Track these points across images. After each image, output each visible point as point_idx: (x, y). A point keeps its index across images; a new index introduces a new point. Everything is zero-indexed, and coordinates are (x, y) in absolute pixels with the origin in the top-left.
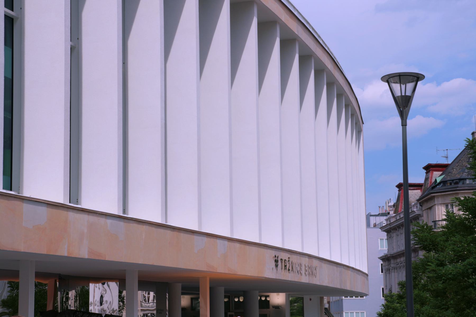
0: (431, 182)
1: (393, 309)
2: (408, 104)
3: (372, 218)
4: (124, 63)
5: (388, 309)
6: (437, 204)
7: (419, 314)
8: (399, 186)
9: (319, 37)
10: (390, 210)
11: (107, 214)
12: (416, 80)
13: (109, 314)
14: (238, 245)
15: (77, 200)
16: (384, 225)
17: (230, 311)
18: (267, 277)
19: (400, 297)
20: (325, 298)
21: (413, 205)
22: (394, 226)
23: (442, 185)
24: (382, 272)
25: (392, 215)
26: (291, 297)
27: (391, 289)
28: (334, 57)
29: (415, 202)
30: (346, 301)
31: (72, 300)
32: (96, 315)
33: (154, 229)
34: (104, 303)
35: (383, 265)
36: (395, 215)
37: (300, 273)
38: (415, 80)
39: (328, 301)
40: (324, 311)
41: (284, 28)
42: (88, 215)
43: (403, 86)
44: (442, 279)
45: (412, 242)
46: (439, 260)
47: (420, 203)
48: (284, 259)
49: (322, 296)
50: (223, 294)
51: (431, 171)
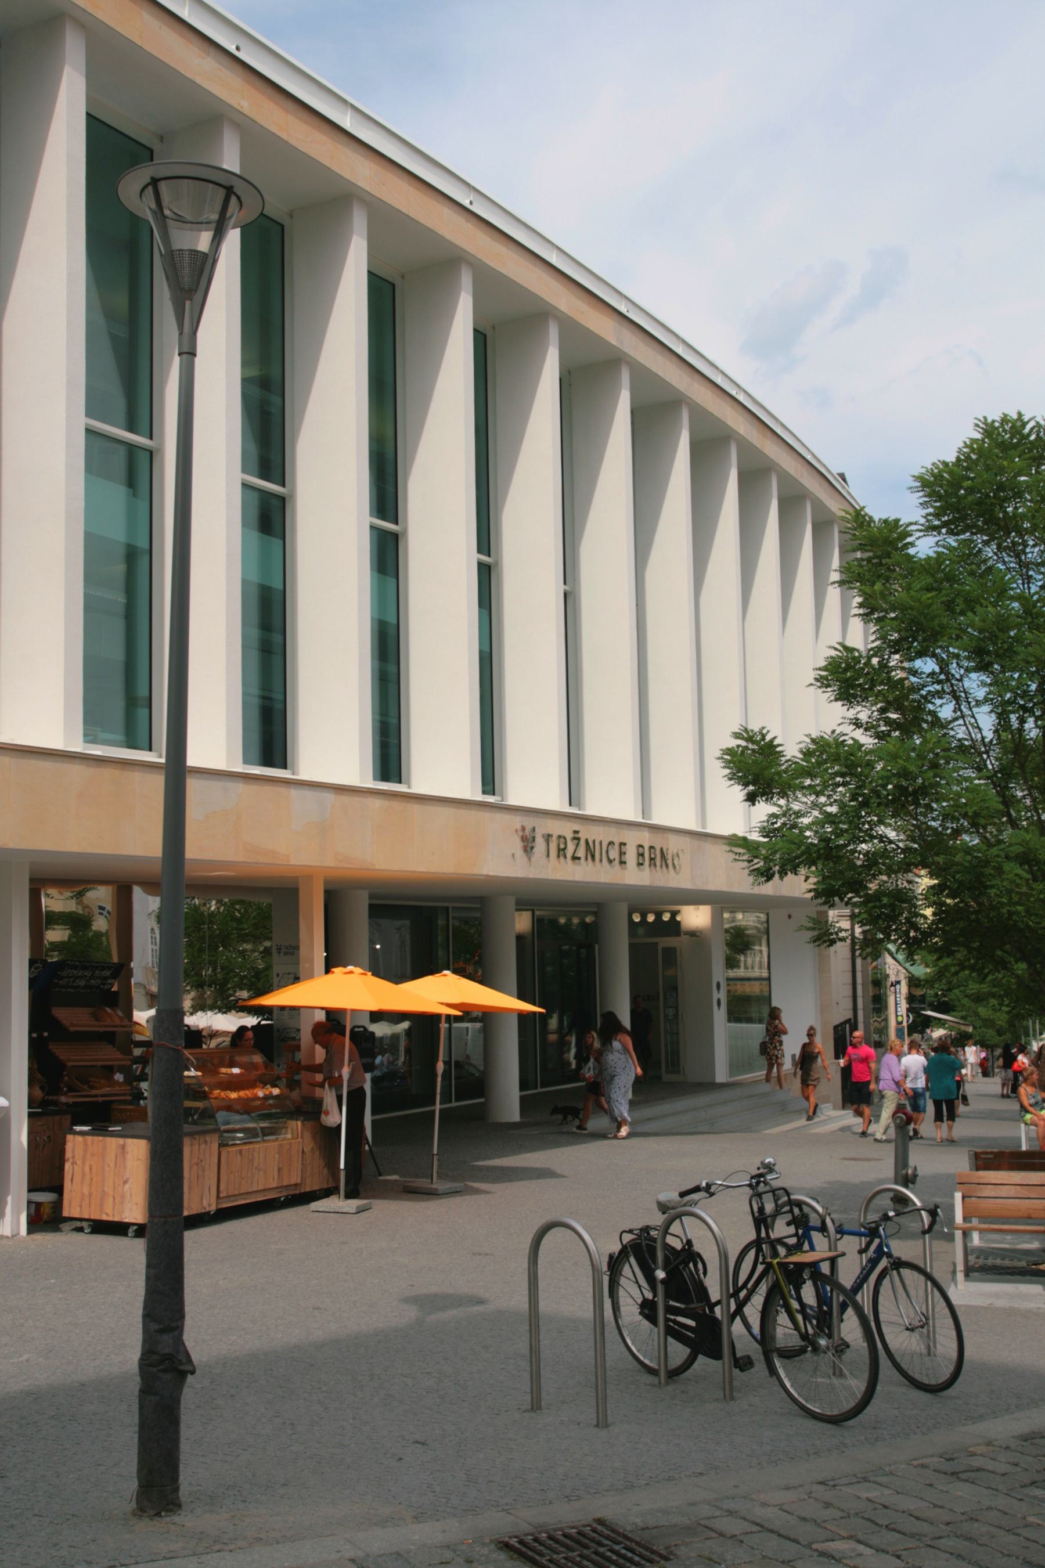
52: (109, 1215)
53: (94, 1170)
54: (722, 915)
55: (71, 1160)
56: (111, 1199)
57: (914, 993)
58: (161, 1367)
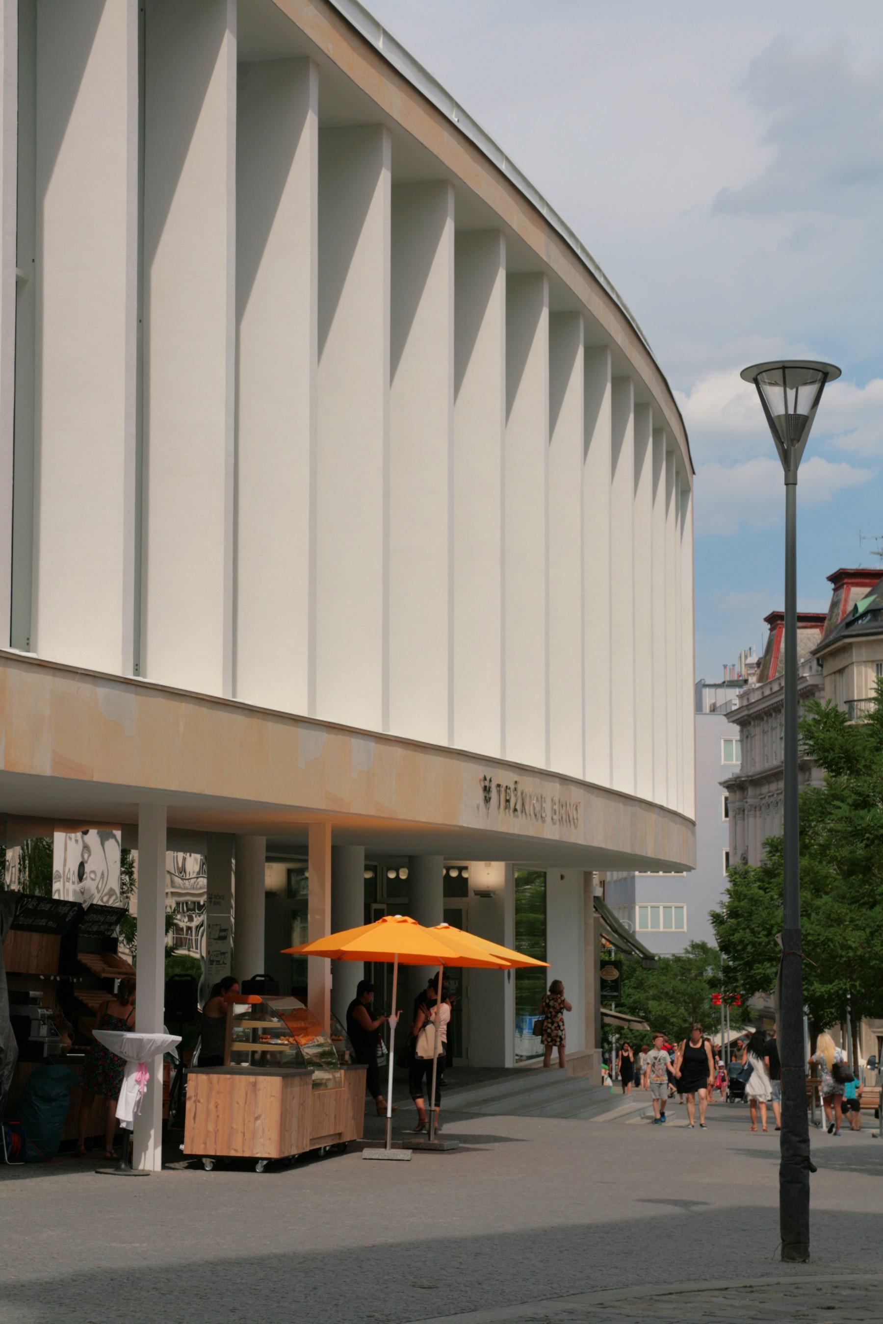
0: (845, 612)
1: (751, 899)
2: (801, 436)
3: (707, 692)
4: (140, 321)
5: (740, 901)
6: (856, 662)
7: (809, 912)
8: (773, 619)
9: (598, 268)
10: (749, 675)
11: (96, 675)
12: (819, 380)
13: (100, 903)
14: (398, 752)
15: (28, 639)
16: (734, 708)
17: (376, 902)
18: (465, 825)
19: (768, 873)
20: (596, 874)
21: (802, 663)
22: (757, 711)
23: (869, 617)
24: (727, 815)
25: (753, 686)
26: (518, 871)
27: (745, 856)
28: (632, 317)
29: (807, 655)
30: (643, 880)
31: (13, 867)
32: (69, 905)
33: (205, 712)
34: (86, 878)
35: (730, 800)
36: (760, 684)
37: (542, 817)
38: (818, 378)
39: (602, 880)
40: (592, 903)
41: (518, 246)
42: (54, 676)
43: (791, 393)
44: (865, 838)
45: (801, 748)
46: (858, 794)
47: (818, 660)
48: (504, 786)
49: (587, 869)
50: (361, 862)
51: (845, 586)
52: (239, 1150)
53: (220, 1107)
54: (409, 875)
55: (193, 1099)
56: (240, 1135)
57: (604, 978)
58: (802, 1165)
